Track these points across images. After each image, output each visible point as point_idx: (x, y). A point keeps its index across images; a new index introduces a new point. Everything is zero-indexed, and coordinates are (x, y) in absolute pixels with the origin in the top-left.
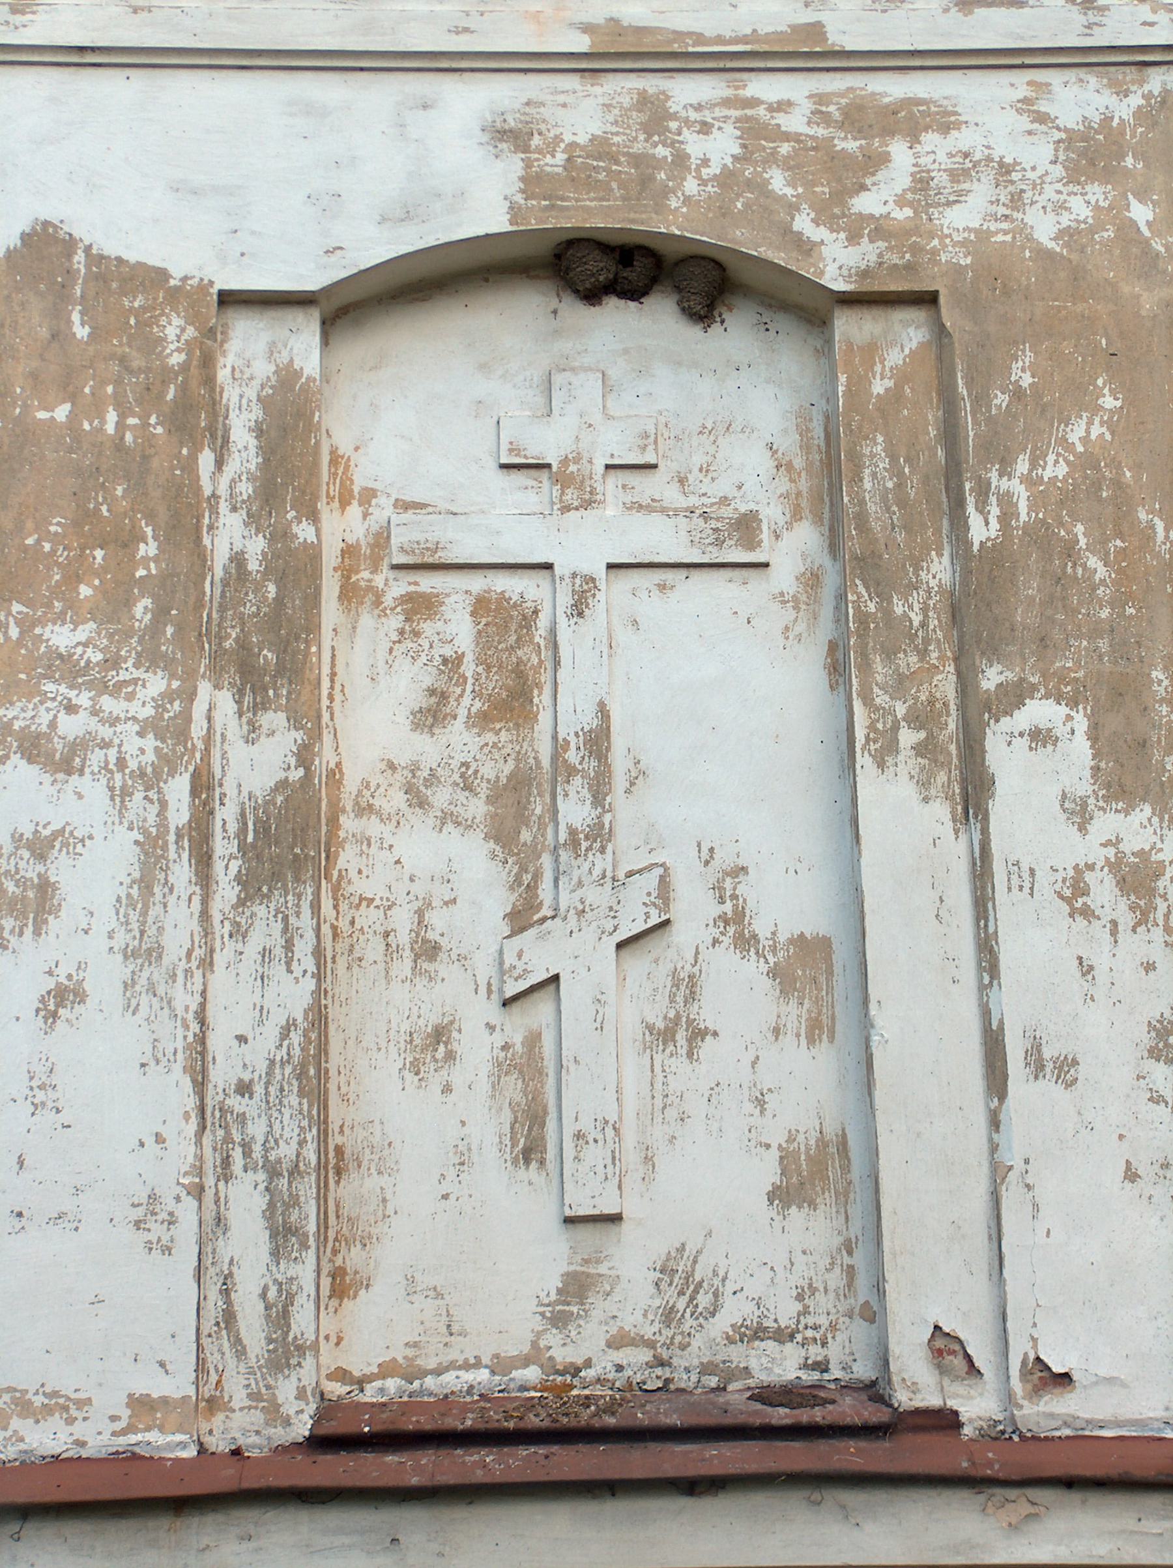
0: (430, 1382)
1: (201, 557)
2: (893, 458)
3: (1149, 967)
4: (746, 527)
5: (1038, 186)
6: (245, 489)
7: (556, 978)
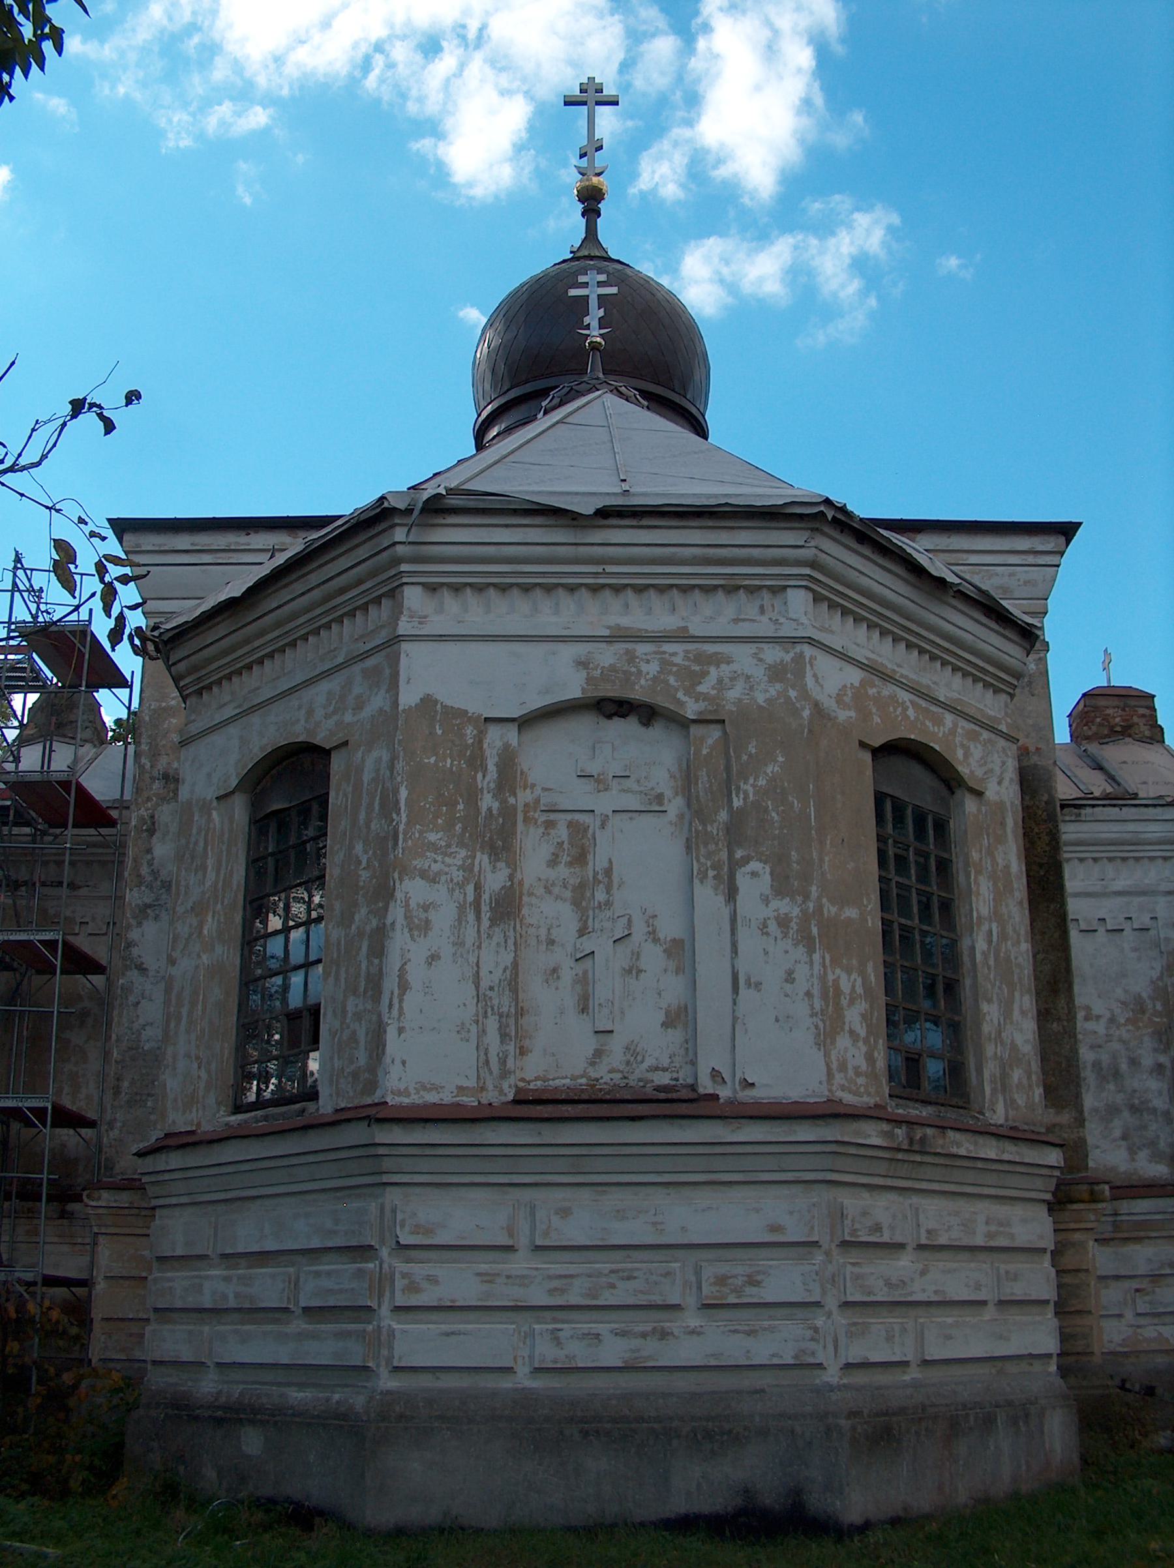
0: (551, 1083)
1: (478, 810)
2: (709, 776)
3: (787, 952)
4: (659, 798)
5: (758, 684)
6: (492, 785)
7: (1067, 530)
